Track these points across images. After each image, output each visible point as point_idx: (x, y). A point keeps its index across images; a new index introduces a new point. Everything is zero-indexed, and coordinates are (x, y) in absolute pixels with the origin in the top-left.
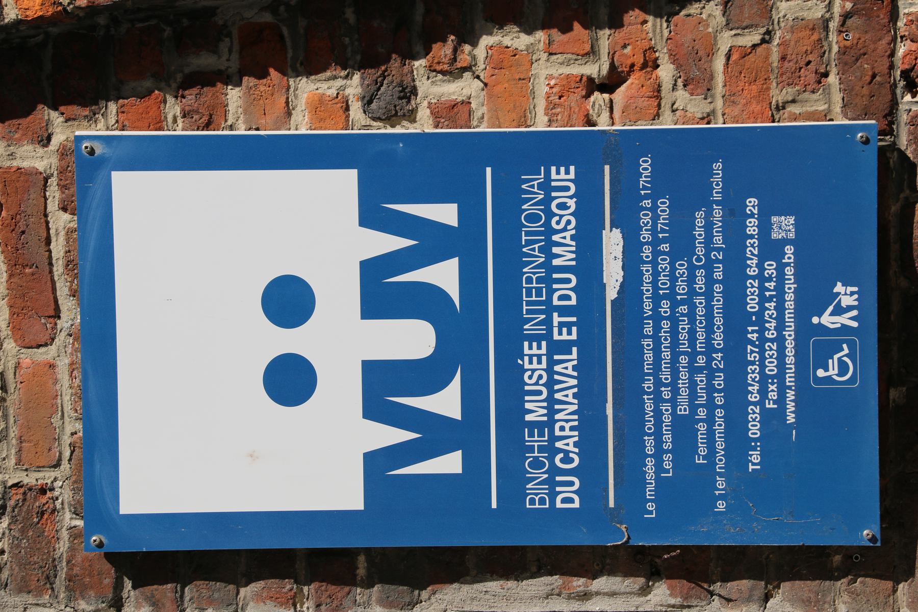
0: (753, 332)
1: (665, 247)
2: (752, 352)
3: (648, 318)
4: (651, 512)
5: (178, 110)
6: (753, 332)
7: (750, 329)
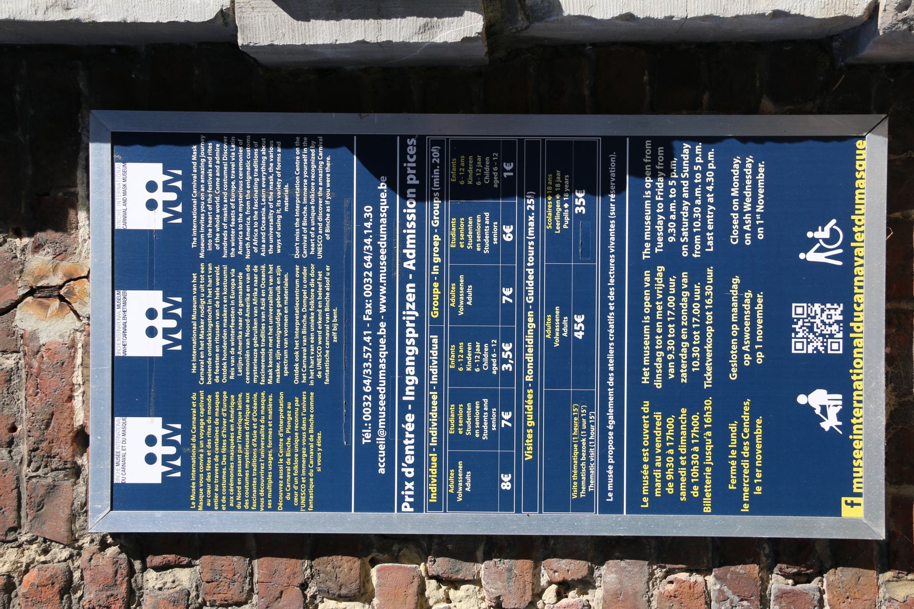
0: (367, 335)
1: (709, 433)
2: (367, 351)
3: (658, 454)
4: (645, 504)
5: (13, 558)
6: (367, 335)
7: (365, 333)
